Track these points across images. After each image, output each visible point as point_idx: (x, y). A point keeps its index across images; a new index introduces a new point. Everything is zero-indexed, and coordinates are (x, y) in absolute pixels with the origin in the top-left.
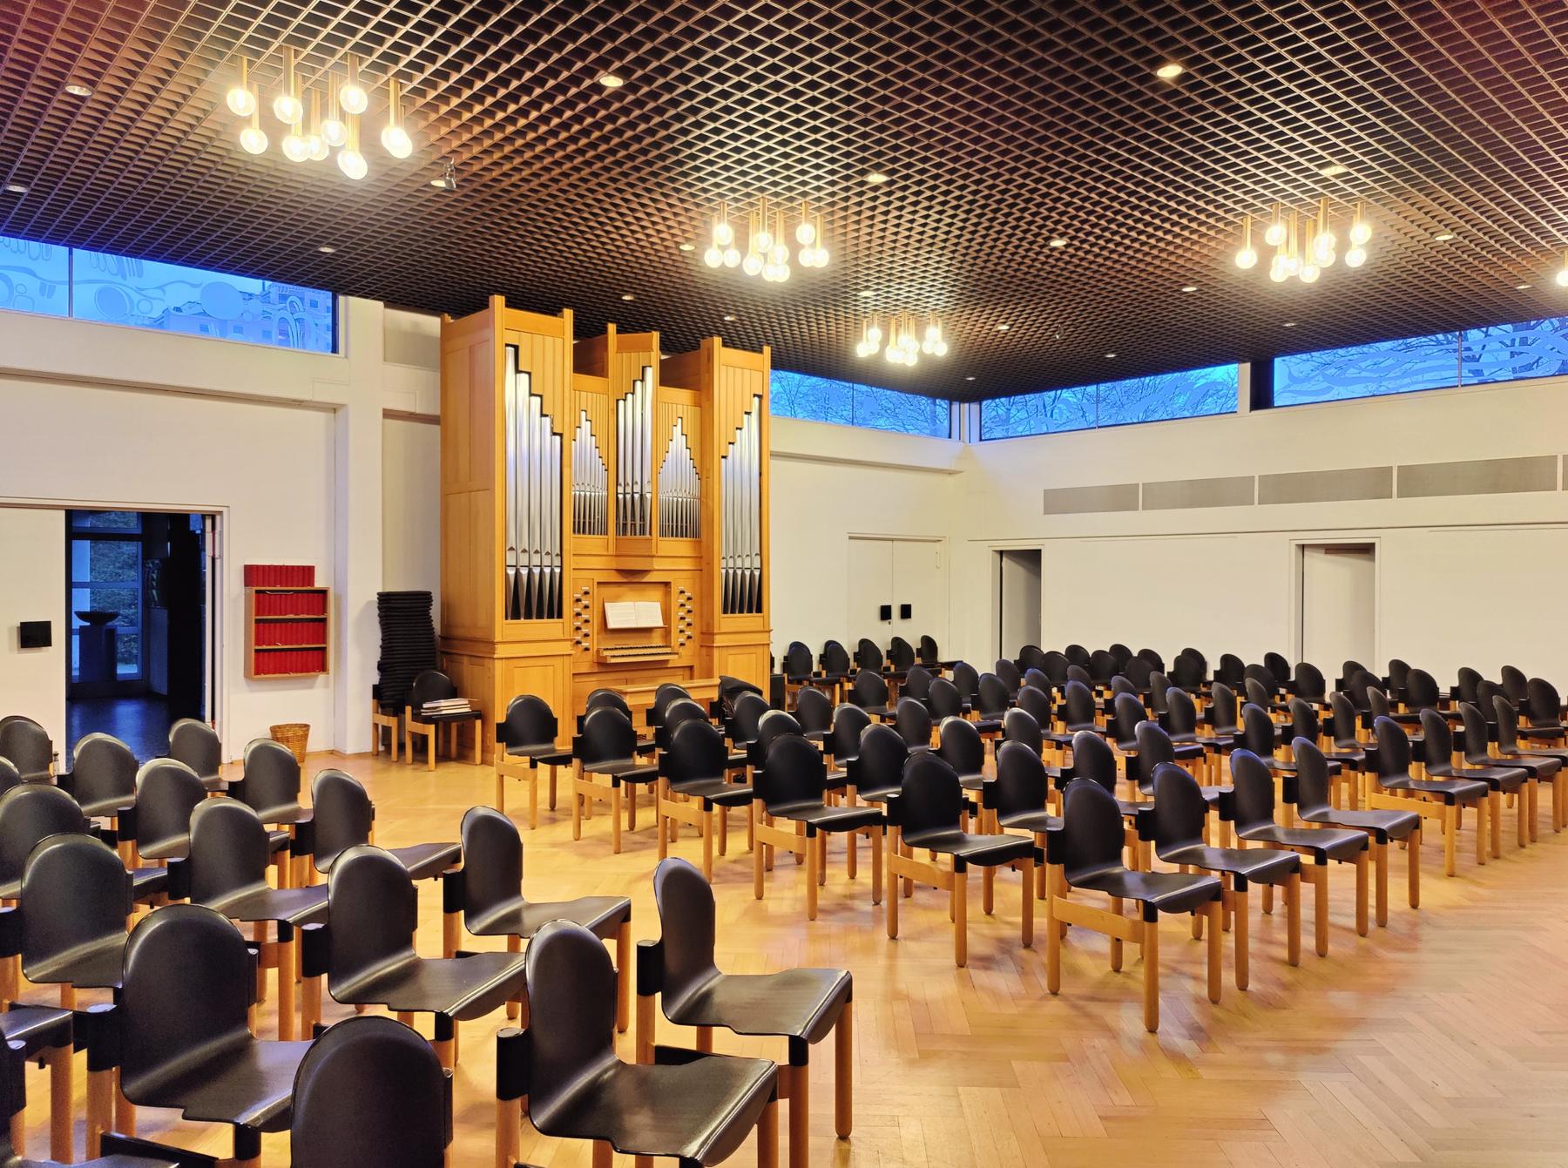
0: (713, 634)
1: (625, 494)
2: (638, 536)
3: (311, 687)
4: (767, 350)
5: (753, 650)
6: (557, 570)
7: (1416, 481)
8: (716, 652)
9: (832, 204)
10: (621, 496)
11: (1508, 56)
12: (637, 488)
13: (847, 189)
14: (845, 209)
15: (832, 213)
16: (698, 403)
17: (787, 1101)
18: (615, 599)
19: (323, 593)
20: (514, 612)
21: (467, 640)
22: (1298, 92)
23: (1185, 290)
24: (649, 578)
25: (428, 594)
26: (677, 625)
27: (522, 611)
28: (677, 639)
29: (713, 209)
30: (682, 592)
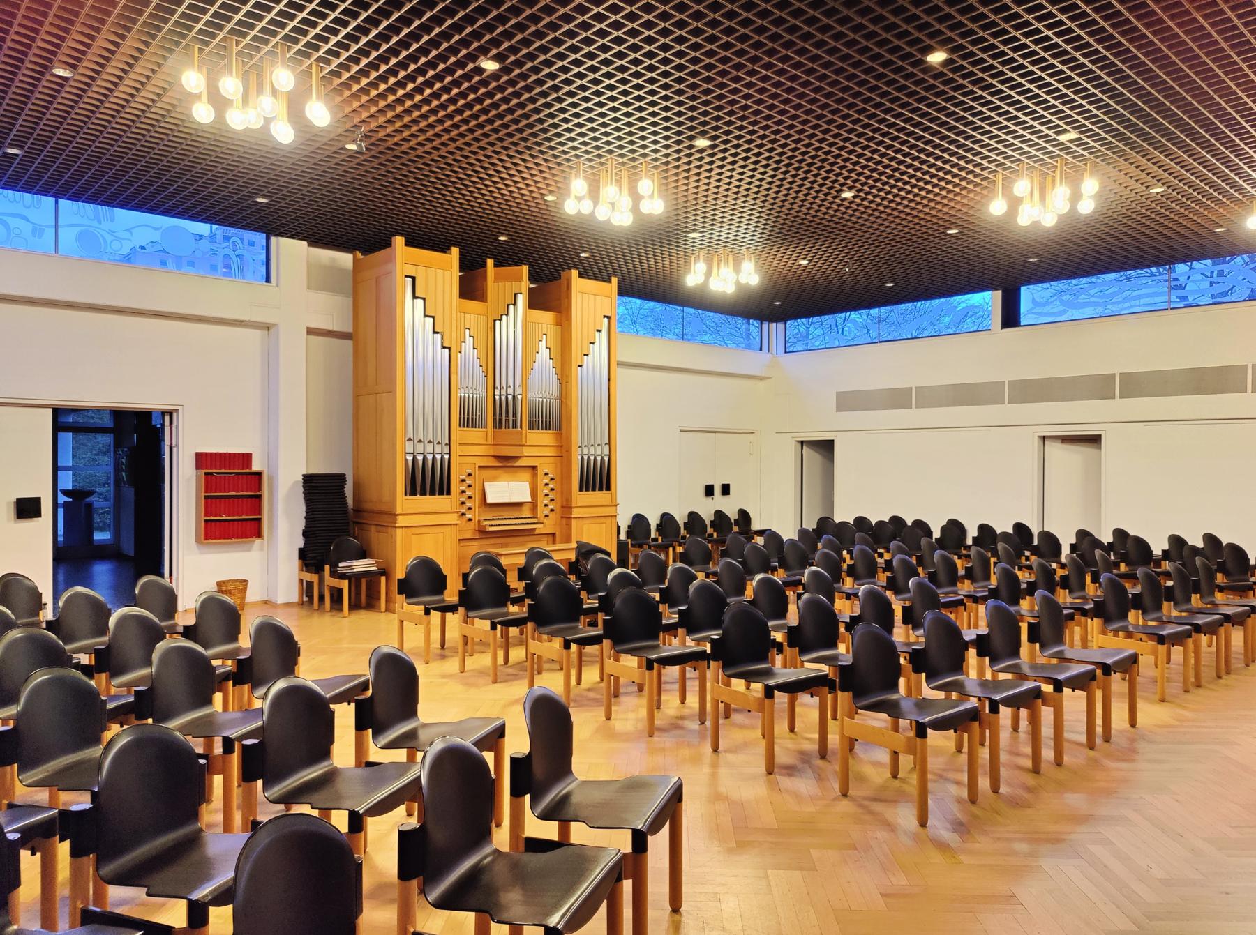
0: (571, 508)
1: (500, 395)
2: (511, 429)
3: (249, 550)
4: (614, 280)
5: (603, 520)
6: (446, 457)
7: (1135, 385)
8: (573, 522)
9: (667, 163)
10: (497, 397)
11: (1208, 45)
12: (510, 391)
13: (678, 151)
14: (677, 167)
15: (666, 171)
16: (559, 323)
17: (630, 881)
18: (493, 479)
19: (259, 475)
20: (412, 490)
21: (374, 512)
22: (1040, 73)
23: (950, 232)
24: (519, 463)
25: (343, 476)
26: (542, 501)
27: (418, 489)
28: (543, 512)
29: (571, 168)
30: (546, 474)
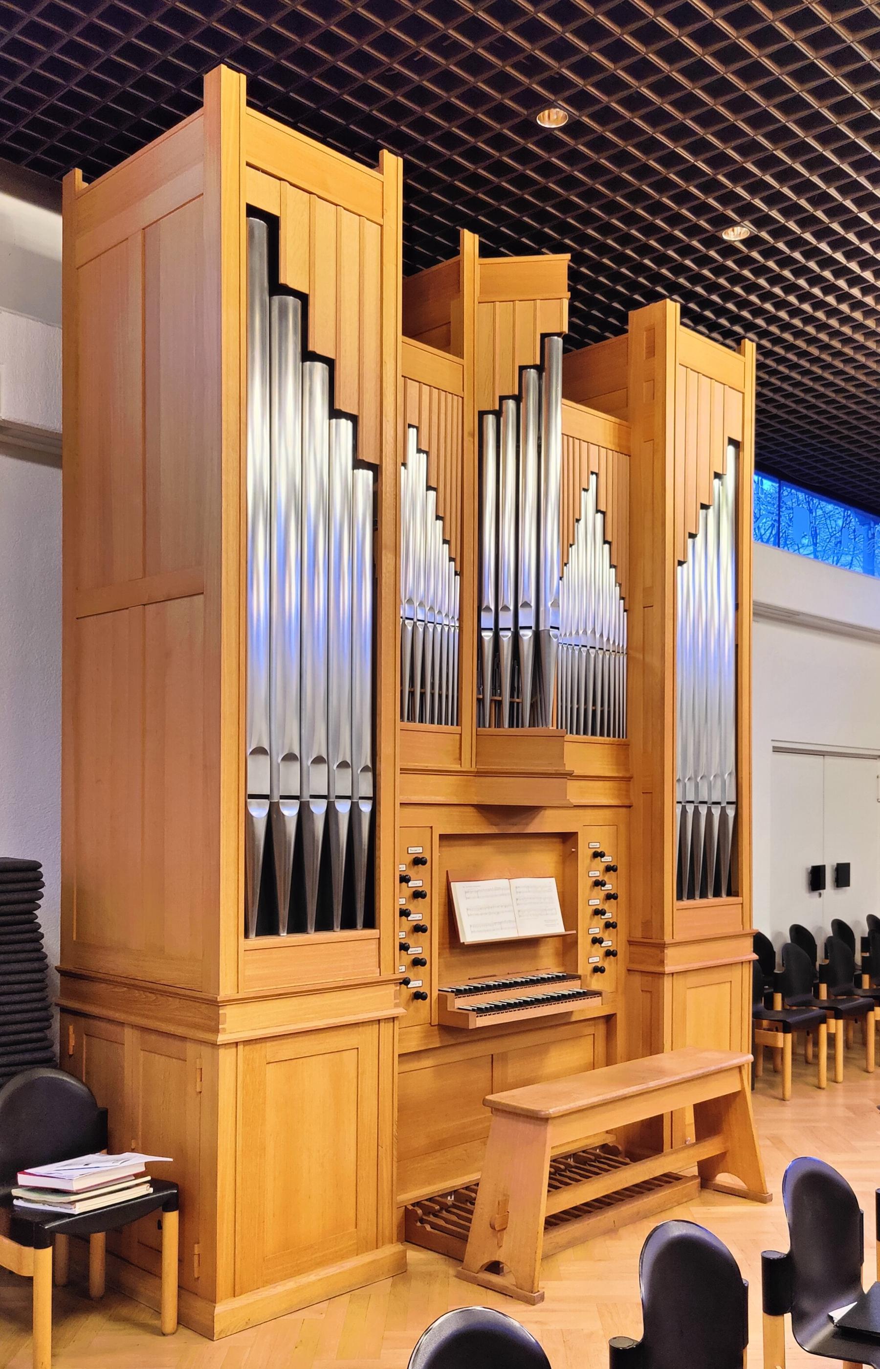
0: (662, 946)
1: (497, 630)
5: (724, 975)
8: (667, 982)
10: (488, 636)
12: (527, 618)
16: (624, 450)
18: (472, 875)
21: (132, 984)
25: (33, 868)
27: (284, 912)
30: (597, 855)
